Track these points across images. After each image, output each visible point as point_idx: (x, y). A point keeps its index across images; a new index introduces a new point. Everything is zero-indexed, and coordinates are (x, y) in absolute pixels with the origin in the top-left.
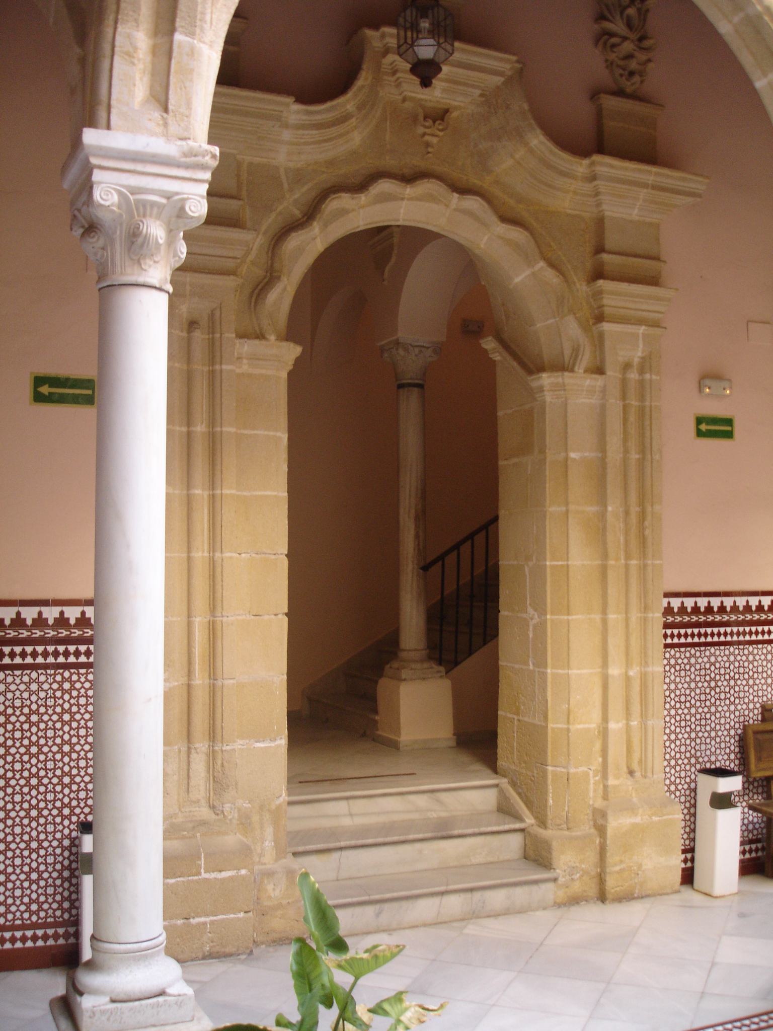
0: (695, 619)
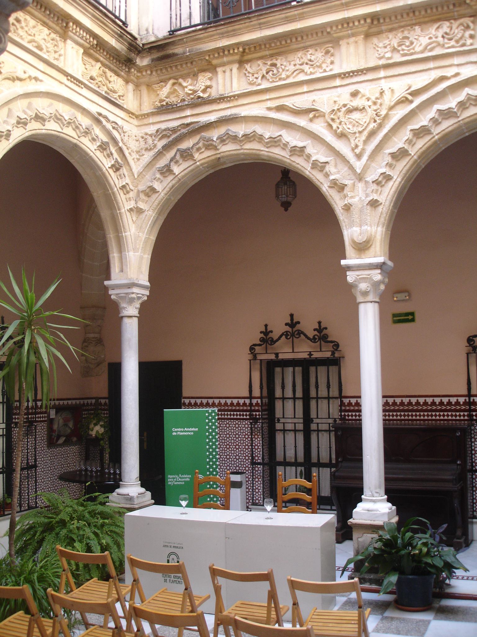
0: (425, 408)
